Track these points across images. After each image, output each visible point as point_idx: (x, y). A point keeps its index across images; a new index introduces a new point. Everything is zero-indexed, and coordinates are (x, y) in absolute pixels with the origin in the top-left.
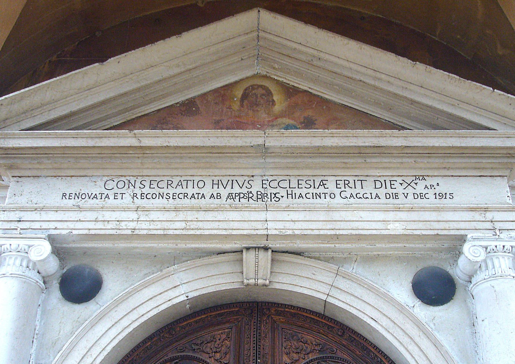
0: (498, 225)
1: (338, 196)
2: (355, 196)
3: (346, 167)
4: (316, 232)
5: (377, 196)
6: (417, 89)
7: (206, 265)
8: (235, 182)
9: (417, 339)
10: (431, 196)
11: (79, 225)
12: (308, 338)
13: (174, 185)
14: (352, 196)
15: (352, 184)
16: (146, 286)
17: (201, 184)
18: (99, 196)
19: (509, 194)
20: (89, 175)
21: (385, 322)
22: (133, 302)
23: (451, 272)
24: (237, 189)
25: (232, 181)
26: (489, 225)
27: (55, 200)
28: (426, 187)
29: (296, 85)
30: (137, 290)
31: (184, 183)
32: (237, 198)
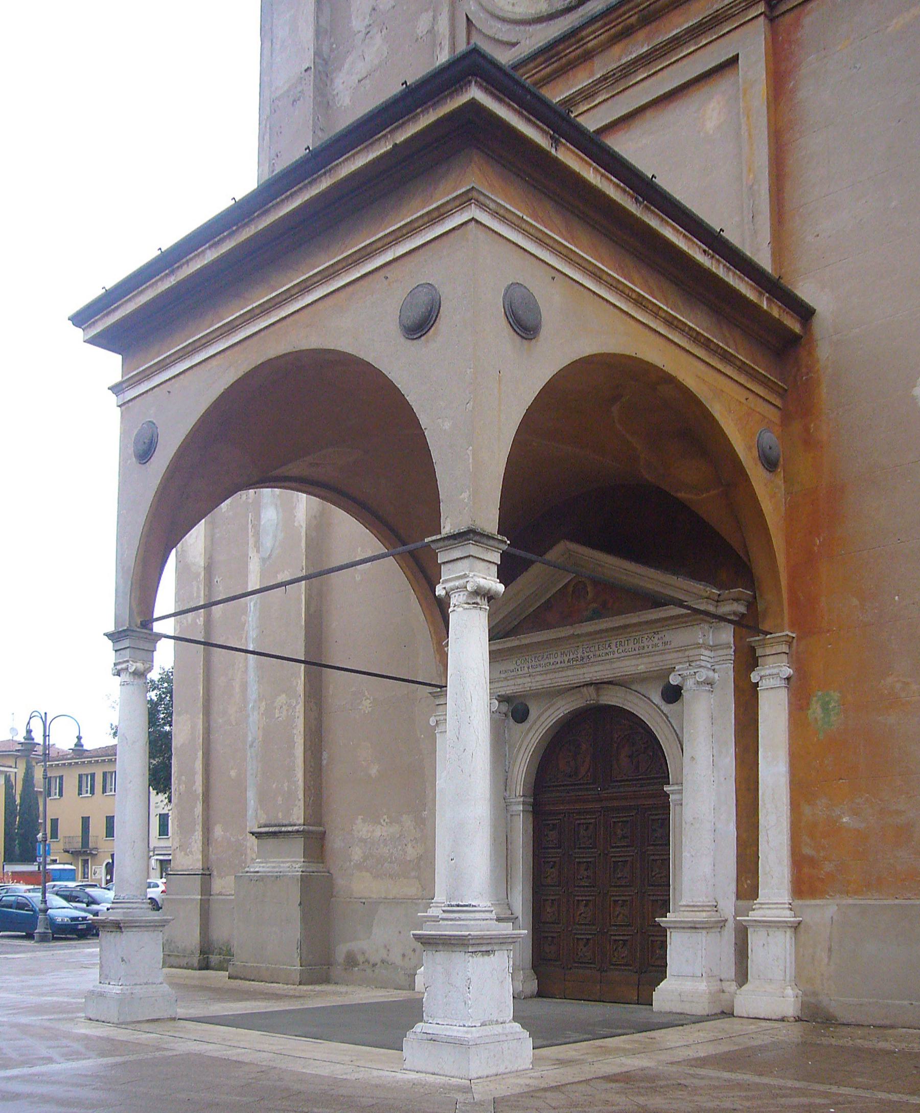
0: (691, 659)
15: (623, 644)
16: (546, 710)
22: (542, 719)
24: (572, 657)
28: (659, 639)
30: (543, 713)
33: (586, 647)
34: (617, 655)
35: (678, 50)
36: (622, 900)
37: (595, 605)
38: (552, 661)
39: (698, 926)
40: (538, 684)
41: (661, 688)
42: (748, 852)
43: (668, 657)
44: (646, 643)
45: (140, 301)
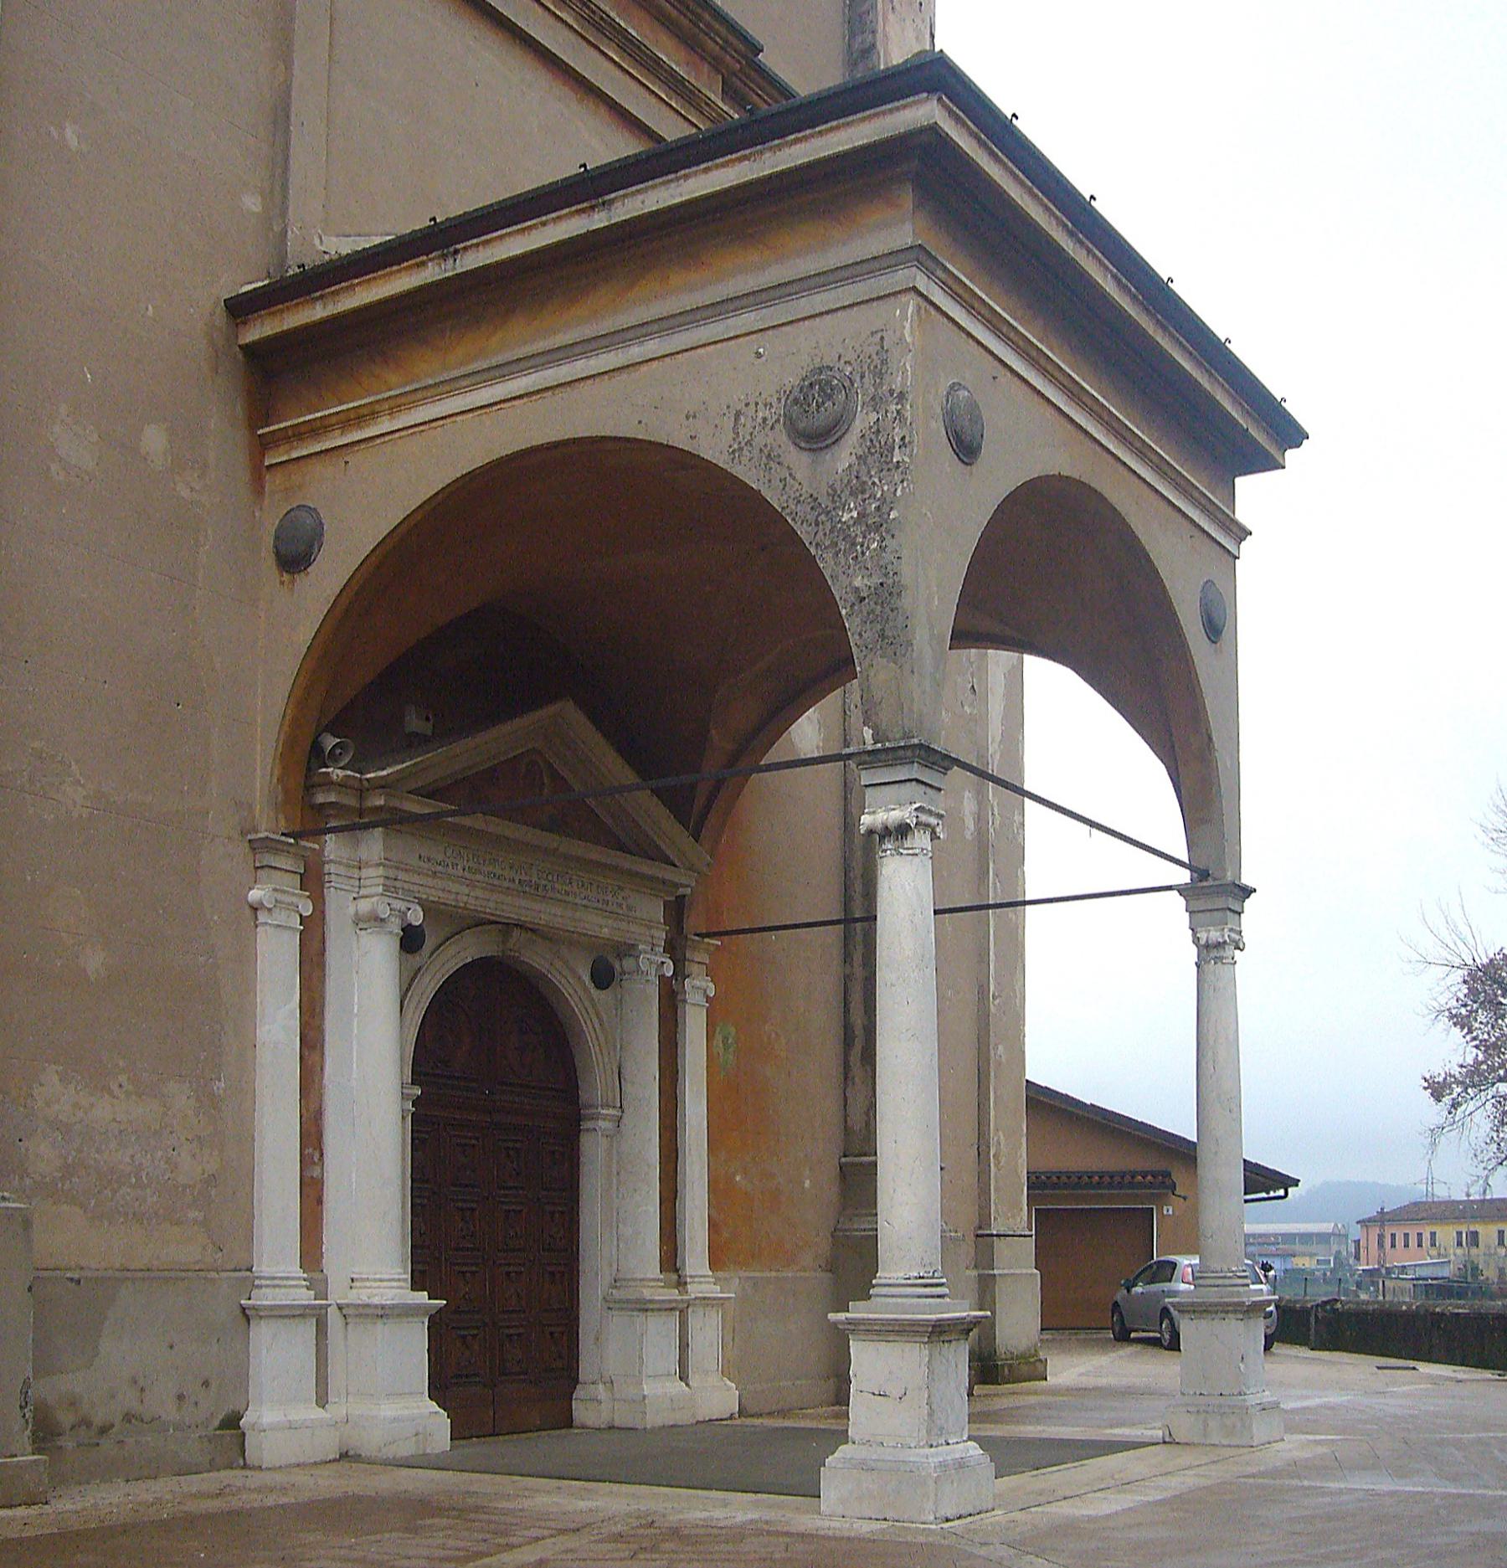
35: (652, 77)
40: (477, 903)
45: (1028, 207)
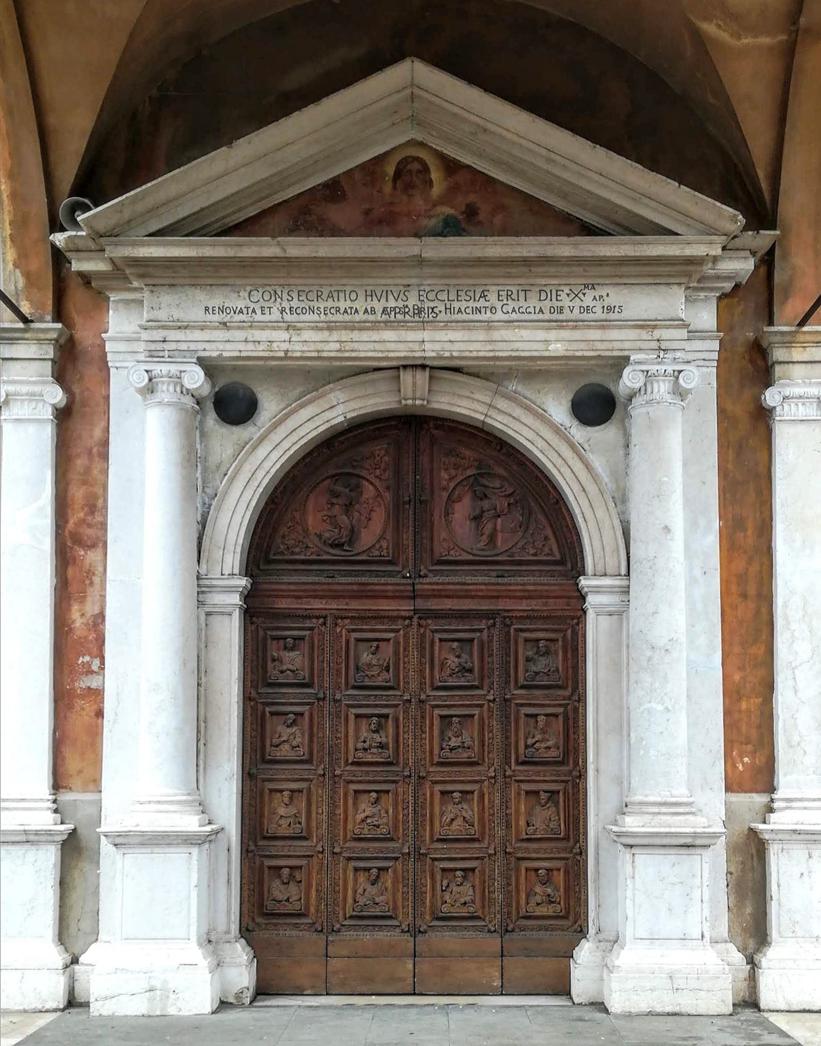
0: (664, 345)
1: (499, 310)
2: (517, 311)
3: (509, 276)
4: (474, 354)
5: (541, 311)
6: (596, 177)
7: (364, 383)
8: (389, 293)
9: (570, 462)
10: (598, 310)
11: (228, 346)
12: (468, 453)
13: (324, 296)
14: (514, 310)
15: (514, 296)
17: (353, 296)
18: (245, 311)
19: (683, 307)
20: (230, 283)
21: (540, 443)
22: (291, 423)
23: (613, 389)
24: (392, 303)
25: (387, 291)
26: (655, 345)
27: (196, 314)
28: (595, 298)
29: (458, 158)
31: (335, 295)
32: (393, 313)
33: (428, 289)
34: (499, 316)
36: (461, 792)
37: (447, 210)
38: (343, 305)
39: (698, 842)
41: (570, 397)
42: (744, 705)
43: (614, 334)
44: (566, 302)
